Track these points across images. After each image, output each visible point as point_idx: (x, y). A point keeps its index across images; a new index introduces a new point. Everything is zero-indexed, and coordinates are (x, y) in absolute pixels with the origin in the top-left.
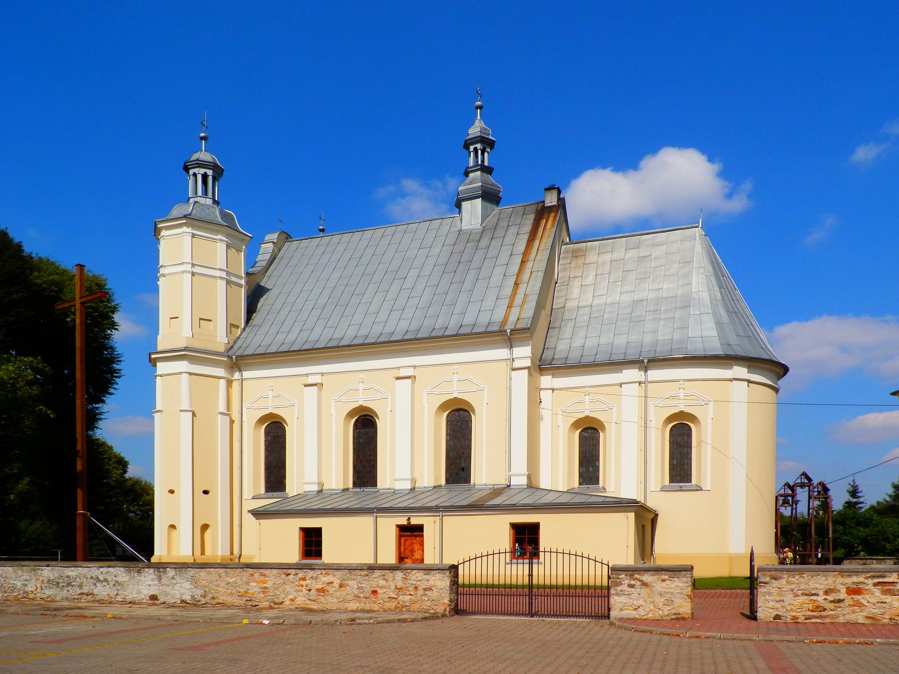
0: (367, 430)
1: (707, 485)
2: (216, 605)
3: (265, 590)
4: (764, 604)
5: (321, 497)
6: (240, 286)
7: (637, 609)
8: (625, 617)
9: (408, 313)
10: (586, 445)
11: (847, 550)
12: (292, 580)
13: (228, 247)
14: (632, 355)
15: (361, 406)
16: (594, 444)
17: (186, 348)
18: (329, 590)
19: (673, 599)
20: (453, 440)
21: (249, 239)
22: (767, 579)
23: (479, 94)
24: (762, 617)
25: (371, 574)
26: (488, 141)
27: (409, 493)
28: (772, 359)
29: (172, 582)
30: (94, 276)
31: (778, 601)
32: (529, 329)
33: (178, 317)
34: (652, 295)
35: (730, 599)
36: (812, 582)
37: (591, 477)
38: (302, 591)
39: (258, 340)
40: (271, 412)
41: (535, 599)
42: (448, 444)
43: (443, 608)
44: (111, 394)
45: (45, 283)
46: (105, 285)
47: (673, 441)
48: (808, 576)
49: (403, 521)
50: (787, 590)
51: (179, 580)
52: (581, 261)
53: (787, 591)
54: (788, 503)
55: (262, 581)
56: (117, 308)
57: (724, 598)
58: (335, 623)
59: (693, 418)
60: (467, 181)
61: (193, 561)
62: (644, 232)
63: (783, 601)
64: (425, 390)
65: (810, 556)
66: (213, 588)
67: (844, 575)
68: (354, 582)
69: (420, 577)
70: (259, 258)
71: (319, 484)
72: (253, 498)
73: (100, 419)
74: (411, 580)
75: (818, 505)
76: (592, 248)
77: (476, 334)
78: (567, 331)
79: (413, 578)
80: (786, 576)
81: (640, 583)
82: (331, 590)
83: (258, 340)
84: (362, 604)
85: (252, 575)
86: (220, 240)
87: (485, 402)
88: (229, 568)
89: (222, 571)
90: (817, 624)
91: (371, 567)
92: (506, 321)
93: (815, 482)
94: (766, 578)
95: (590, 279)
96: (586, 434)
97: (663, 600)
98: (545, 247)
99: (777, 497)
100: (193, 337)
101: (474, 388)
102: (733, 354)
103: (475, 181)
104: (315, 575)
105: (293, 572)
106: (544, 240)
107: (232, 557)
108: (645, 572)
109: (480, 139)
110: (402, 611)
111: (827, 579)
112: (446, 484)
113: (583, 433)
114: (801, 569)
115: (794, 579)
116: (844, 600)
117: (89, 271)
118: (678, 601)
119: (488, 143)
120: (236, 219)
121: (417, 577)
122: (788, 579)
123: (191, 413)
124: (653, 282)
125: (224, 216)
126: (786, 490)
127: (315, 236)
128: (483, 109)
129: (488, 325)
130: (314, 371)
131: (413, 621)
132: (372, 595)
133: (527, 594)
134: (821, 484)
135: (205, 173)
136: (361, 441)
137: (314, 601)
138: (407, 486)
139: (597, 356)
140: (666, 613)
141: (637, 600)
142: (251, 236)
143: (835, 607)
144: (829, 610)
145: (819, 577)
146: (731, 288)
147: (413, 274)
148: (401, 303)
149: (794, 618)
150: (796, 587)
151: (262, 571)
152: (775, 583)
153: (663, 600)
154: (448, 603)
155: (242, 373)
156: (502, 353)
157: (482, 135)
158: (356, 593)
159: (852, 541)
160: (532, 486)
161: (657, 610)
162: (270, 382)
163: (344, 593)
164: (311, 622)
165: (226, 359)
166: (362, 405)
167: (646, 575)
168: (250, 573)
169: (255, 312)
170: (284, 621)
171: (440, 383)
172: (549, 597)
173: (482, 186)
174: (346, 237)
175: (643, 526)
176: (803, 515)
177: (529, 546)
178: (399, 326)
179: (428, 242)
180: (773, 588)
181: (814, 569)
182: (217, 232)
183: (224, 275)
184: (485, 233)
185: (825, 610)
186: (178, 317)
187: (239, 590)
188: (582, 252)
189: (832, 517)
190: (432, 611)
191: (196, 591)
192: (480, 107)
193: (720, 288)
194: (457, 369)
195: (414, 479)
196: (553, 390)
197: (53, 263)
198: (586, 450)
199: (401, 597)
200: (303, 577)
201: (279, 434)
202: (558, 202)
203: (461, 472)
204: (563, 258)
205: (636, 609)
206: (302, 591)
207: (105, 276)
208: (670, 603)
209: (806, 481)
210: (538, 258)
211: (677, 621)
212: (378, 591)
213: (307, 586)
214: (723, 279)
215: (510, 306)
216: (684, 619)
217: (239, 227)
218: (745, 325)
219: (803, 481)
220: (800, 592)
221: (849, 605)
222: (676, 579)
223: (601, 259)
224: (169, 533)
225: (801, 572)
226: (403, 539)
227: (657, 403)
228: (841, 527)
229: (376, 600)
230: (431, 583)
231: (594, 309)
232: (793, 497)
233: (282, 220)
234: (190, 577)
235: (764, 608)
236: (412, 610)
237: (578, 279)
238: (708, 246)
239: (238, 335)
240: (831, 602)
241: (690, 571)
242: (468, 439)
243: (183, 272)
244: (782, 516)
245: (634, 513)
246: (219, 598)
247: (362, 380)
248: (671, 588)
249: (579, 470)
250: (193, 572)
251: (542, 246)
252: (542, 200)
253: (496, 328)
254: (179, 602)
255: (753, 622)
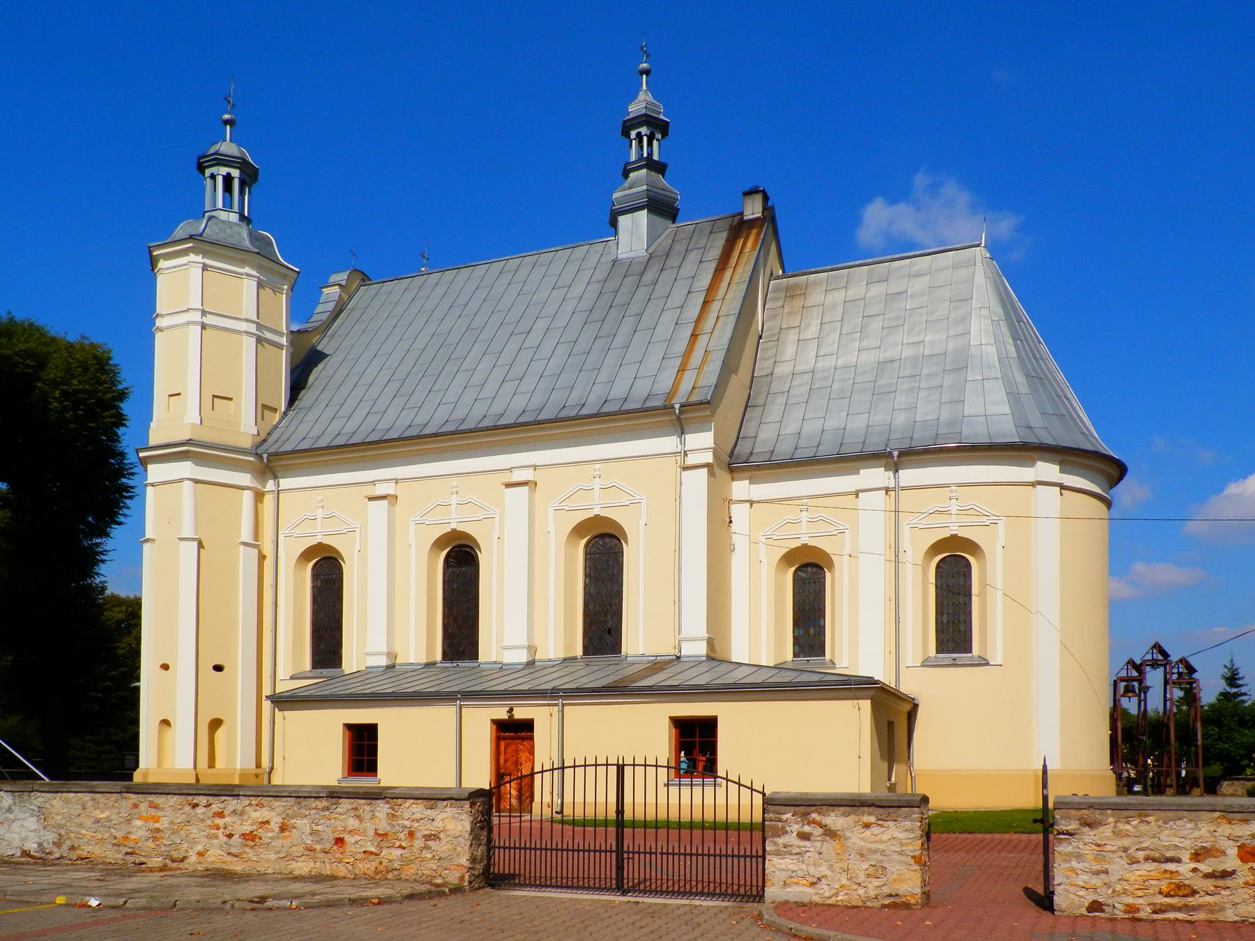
0: (464, 569)
1: (996, 656)
2: (77, 862)
3: (156, 834)
4: (1068, 877)
5: (392, 674)
6: (280, 346)
7: (816, 883)
8: (792, 900)
9: (528, 385)
10: (804, 592)
11: (1226, 765)
12: (201, 817)
13: (260, 285)
14: (874, 445)
15: (454, 531)
16: (817, 590)
17: (191, 442)
18: (263, 835)
19: (886, 865)
20: (595, 584)
21: (295, 275)
22: (1073, 826)
23: (645, 52)
24: (1064, 906)
25: (334, 807)
26: (660, 123)
27: (524, 669)
28: (1098, 450)
29: (7, 818)
30: (92, 345)
31: (1098, 873)
32: (708, 403)
33: (179, 394)
34: (908, 352)
35: (1021, 855)
36: (1167, 832)
37: (812, 643)
38: (217, 837)
39: (303, 429)
40: (320, 541)
41: (628, 859)
42: (587, 591)
43: (458, 875)
44: (120, 524)
45: (17, 354)
46: (110, 359)
47: (942, 585)
48: (1158, 820)
49: (502, 714)
50: (1114, 848)
51: (20, 814)
52: (798, 303)
53: (1113, 852)
54: (1134, 692)
55: (153, 817)
56: (126, 393)
57: (1010, 852)
58: (221, 906)
59: (973, 547)
60: (626, 185)
61: (193, 781)
62: (896, 256)
63: (1107, 873)
64: (550, 505)
65: (1168, 774)
66: (73, 829)
67: (1233, 819)
68: (305, 821)
69: (418, 812)
70: (319, 308)
71: (389, 654)
72: (292, 678)
73: (103, 561)
74: (403, 819)
75: (1181, 698)
76: (816, 283)
77: (628, 413)
78: (775, 410)
79: (407, 814)
80: (1111, 820)
81: (820, 831)
82: (266, 835)
83: (303, 429)
84: (318, 864)
85: (136, 806)
86: (248, 275)
87: (643, 522)
88: (99, 793)
89: (87, 798)
90: (1177, 924)
91: (333, 792)
92: (675, 391)
93: (1174, 658)
94: (1070, 824)
95: (812, 331)
96: (804, 575)
97: (865, 866)
98: (740, 279)
99: (1115, 681)
100: (201, 423)
101: (626, 500)
102: (1035, 441)
103: (637, 183)
104: (239, 808)
105: (203, 800)
106: (740, 270)
107: (258, 771)
108: (831, 808)
109: (645, 119)
110: (386, 879)
111: (1197, 828)
112: (584, 655)
113: (799, 573)
114: (1142, 804)
115: (1128, 827)
116: (1234, 872)
117: (85, 337)
118: (895, 869)
119: (659, 127)
120: (275, 246)
121: (414, 813)
122: (1115, 827)
123: (195, 544)
124: (908, 332)
125: (254, 237)
126: (1129, 671)
127: (404, 276)
128: (651, 75)
129: (646, 399)
130: (383, 476)
131: (381, 902)
132: (335, 847)
133: (614, 848)
134: (1184, 662)
135: (229, 174)
136: (455, 587)
137: (237, 856)
138: (522, 657)
139: (820, 448)
140: (872, 893)
141: (815, 865)
142: (298, 270)
143: (1216, 887)
144: (1202, 893)
145: (1180, 823)
146: (1033, 341)
147: (541, 324)
148: (517, 370)
149: (1131, 909)
150: (1134, 844)
151: (152, 798)
152: (1090, 835)
153: (865, 866)
154: (467, 864)
155: (279, 482)
156: (669, 443)
157: (648, 113)
158: (308, 842)
159: (1232, 751)
160: (714, 657)
161: (855, 887)
162: (320, 495)
163: (287, 842)
164: (175, 905)
165: (252, 459)
166: (455, 529)
167: (833, 814)
168: (133, 801)
169: (304, 388)
170: (126, 902)
171: (571, 493)
172: (653, 856)
173: (647, 190)
174: (449, 275)
175: (891, 724)
176: (1159, 713)
177: (703, 756)
178: (512, 404)
179: (565, 280)
180: (1085, 844)
181: (1170, 805)
182: (242, 263)
183: (252, 328)
184: (652, 262)
185: (1194, 893)
186: (179, 394)
187: (114, 834)
188: (801, 290)
189: (1201, 713)
190: (439, 881)
191: (45, 835)
192: (647, 72)
193: (1015, 339)
194: (599, 470)
195: (533, 647)
196: (752, 503)
197: (38, 329)
198: (804, 601)
199: (385, 852)
200: (220, 810)
201: (334, 576)
202: (763, 213)
203: (607, 636)
204: (772, 299)
205: (813, 884)
206: (217, 837)
207: (110, 346)
208: (881, 872)
209: (1160, 657)
210: (729, 295)
211: (891, 912)
212: (346, 839)
213: (225, 828)
214: (1020, 326)
215: (682, 370)
216: (907, 906)
217: (279, 257)
218: (1055, 397)
219: (1155, 657)
220: (1141, 855)
221: (1247, 883)
222: (891, 824)
223: (829, 300)
224: (160, 734)
225: (1142, 811)
226: (503, 744)
227: (915, 521)
228: (1216, 729)
229: (341, 856)
230: (438, 824)
231: (818, 376)
232: (1141, 681)
233: (357, 254)
234: (36, 809)
235: (1068, 887)
236: (403, 876)
237: (793, 331)
238: (995, 275)
239: (275, 423)
240: (1207, 876)
241: (918, 807)
242: (618, 583)
243: (189, 323)
244: (1125, 713)
245: (869, 701)
246: (82, 847)
247: (455, 490)
248: (881, 842)
249: (793, 632)
250: (42, 799)
251: (737, 277)
252: (740, 211)
253: (658, 402)
254: (19, 854)
255: (1047, 914)
